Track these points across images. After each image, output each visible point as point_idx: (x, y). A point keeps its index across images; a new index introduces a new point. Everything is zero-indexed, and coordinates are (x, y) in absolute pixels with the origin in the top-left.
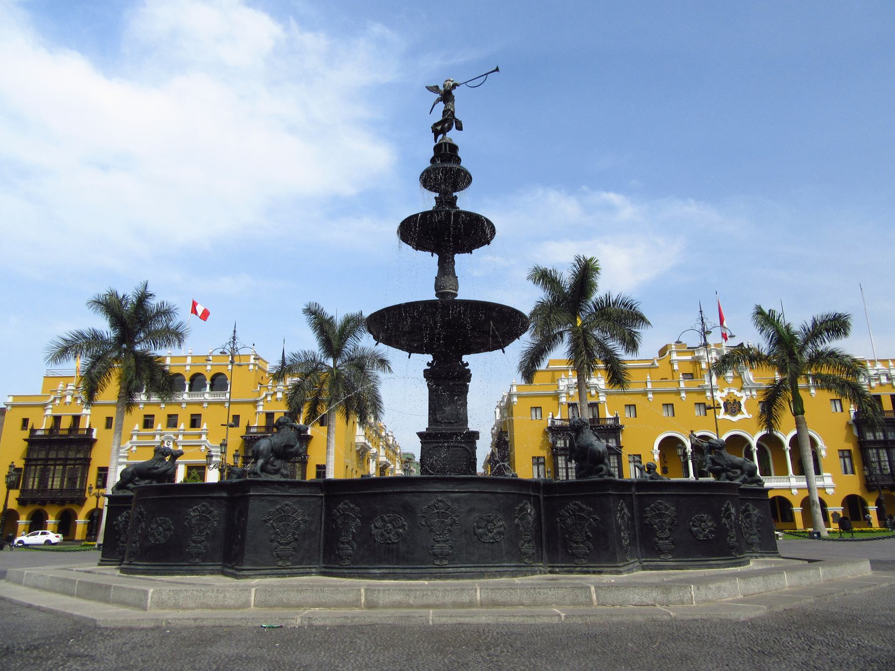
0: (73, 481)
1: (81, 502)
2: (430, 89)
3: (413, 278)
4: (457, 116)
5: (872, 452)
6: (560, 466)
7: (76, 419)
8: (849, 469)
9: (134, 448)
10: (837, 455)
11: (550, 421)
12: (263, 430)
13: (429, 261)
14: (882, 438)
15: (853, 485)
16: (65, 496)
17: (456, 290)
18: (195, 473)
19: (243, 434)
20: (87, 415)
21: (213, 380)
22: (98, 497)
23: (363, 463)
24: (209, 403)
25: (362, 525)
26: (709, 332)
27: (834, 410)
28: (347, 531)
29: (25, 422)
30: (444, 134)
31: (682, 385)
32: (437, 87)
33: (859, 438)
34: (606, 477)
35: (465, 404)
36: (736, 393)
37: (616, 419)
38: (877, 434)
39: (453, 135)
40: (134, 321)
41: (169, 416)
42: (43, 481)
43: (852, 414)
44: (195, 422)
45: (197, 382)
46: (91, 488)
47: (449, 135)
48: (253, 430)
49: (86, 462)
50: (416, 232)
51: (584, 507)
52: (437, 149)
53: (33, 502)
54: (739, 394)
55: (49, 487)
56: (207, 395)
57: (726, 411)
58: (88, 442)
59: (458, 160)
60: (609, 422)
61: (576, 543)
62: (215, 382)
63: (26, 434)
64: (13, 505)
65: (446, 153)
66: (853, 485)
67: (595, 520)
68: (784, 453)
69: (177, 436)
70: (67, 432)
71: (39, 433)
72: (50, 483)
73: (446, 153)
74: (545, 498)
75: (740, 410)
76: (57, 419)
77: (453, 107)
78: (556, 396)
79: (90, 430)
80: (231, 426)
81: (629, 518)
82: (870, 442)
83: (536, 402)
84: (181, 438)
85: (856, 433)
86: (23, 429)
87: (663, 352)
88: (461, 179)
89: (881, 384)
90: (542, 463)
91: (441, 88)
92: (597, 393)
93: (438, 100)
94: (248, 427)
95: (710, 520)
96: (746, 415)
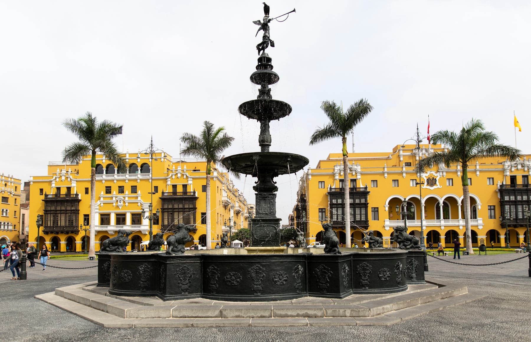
0: (71, 221)
1: (77, 232)
2: (255, 23)
3: (245, 137)
4: (271, 38)
5: (507, 207)
7: (69, 189)
9: (102, 204)
10: (487, 208)
11: (329, 189)
13: (255, 125)
14: (514, 199)
15: (493, 224)
16: (68, 229)
17: (270, 142)
18: (136, 220)
19: (160, 196)
21: (142, 167)
24: (141, 180)
25: (220, 278)
26: (421, 141)
28: (214, 279)
29: (41, 190)
30: (264, 51)
31: (404, 169)
32: (259, 21)
33: (501, 199)
34: (338, 254)
35: (273, 204)
37: (366, 188)
39: (269, 51)
40: (95, 135)
41: (119, 187)
42: (55, 222)
43: (499, 186)
44: (134, 189)
45: (133, 168)
46: (81, 226)
47: (266, 51)
48: (165, 194)
49: (77, 212)
50: (248, 109)
51: (322, 276)
52: (260, 60)
53: (52, 233)
54: (436, 175)
55: (59, 225)
56: (139, 175)
57: (428, 184)
59: (272, 67)
60: (362, 190)
61: (322, 283)
62: (143, 168)
63: (43, 197)
64: (41, 234)
65: (265, 62)
66: (493, 224)
67: (331, 273)
68: (458, 207)
69: (125, 198)
70: (64, 196)
71: (49, 197)
72: (59, 223)
73: (265, 62)
74: (308, 262)
75: (435, 184)
76: (59, 189)
77: (269, 34)
78: (333, 175)
79: (77, 195)
80: (154, 193)
81: (348, 271)
82: (507, 201)
84: (127, 199)
85: (499, 197)
86: (41, 194)
87: (395, 150)
88: (272, 78)
89: (517, 169)
91: (262, 22)
92: (356, 173)
93: (259, 30)
94: (163, 193)
95: (389, 271)
96: (439, 187)
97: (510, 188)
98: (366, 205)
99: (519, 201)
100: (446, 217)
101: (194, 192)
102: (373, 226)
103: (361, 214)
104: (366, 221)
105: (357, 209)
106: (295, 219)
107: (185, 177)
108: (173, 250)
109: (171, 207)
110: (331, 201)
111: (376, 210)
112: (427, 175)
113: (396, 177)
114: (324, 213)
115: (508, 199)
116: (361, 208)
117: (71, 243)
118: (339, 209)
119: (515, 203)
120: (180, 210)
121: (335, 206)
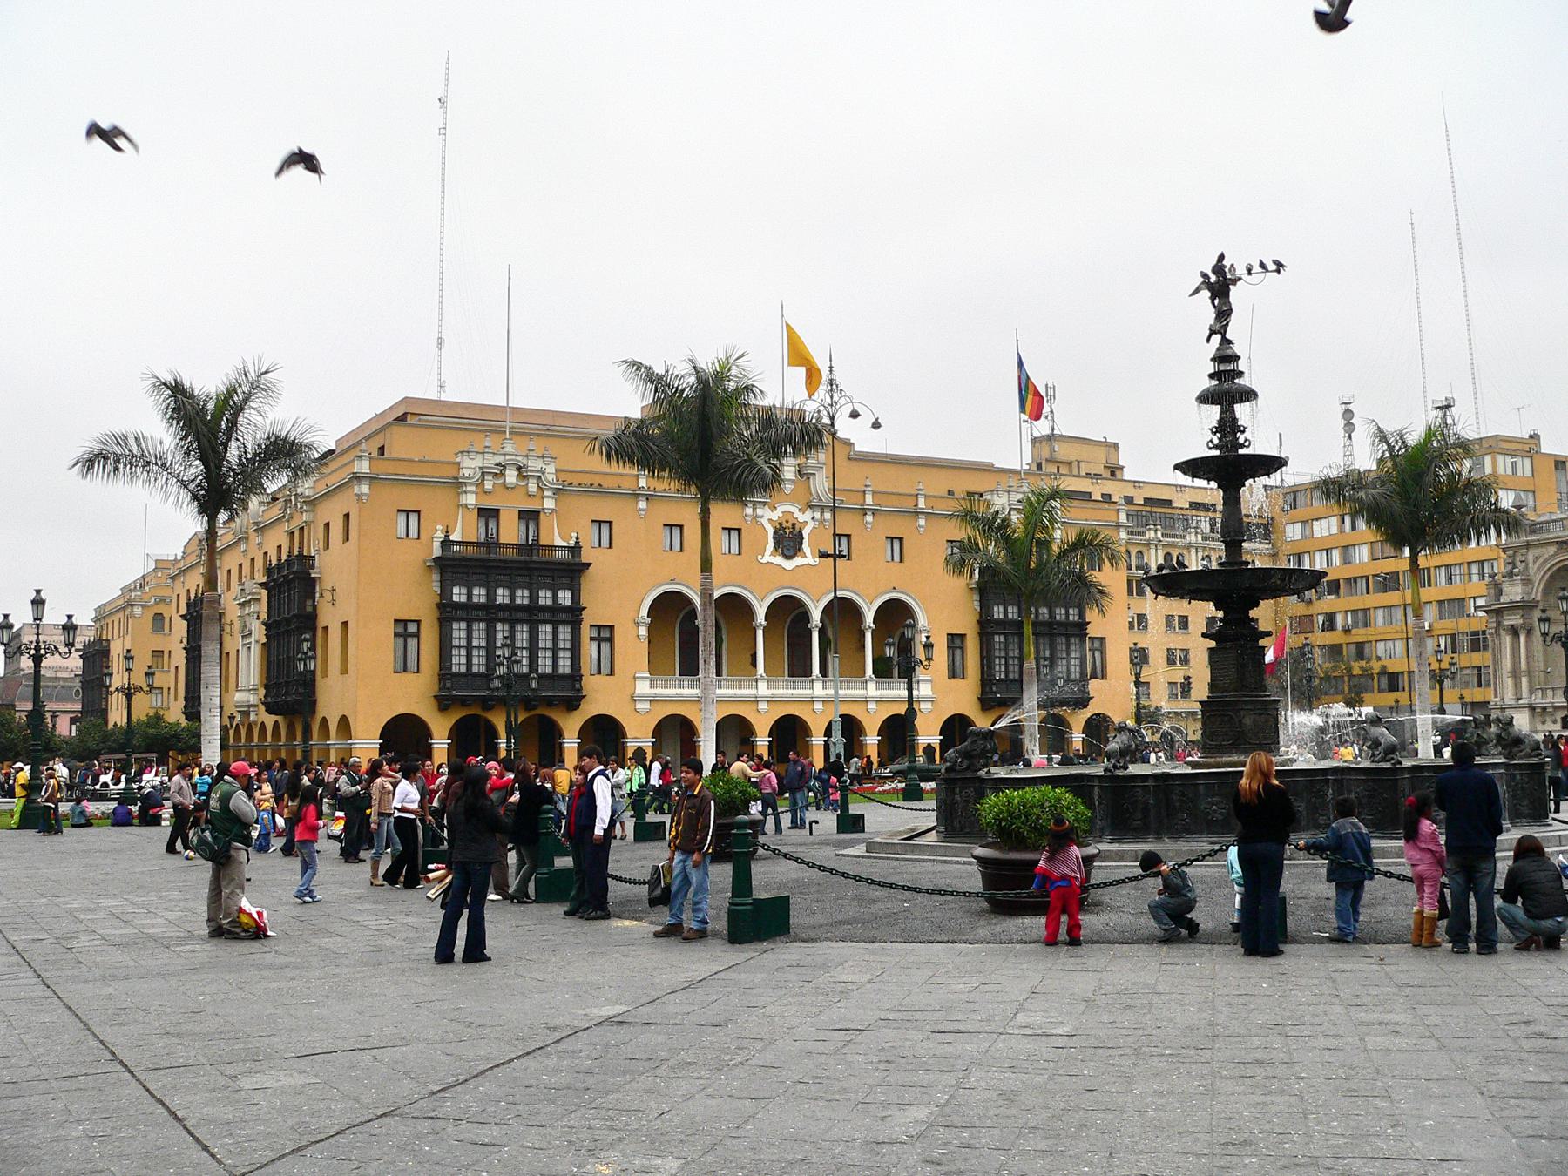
6: (456, 643)
8: (412, 664)
11: (437, 544)
14: (568, 602)
15: (413, 695)
22: (129, 696)
23: (162, 629)
27: (401, 531)
36: (797, 514)
37: (575, 550)
38: (561, 594)
53: (463, 702)
54: (801, 517)
60: (560, 555)
65: (1225, 356)
66: (413, 695)
82: (999, 622)
83: (410, 499)
88: (1249, 395)
90: (605, 640)
97: (516, 557)
98: (573, 615)
102: (601, 698)
103: (555, 650)
104: (575, 676)
108: (1115, 767)
110: (445, 592)
111: (605, 634)
112: (775, 515)
113: (897, 527)
114: (412, 643)
115: (464, 599)
116: (470, 622)
118: (475, 626)
119: (489, 613)
120: (562, 616)
121: (506, 615)
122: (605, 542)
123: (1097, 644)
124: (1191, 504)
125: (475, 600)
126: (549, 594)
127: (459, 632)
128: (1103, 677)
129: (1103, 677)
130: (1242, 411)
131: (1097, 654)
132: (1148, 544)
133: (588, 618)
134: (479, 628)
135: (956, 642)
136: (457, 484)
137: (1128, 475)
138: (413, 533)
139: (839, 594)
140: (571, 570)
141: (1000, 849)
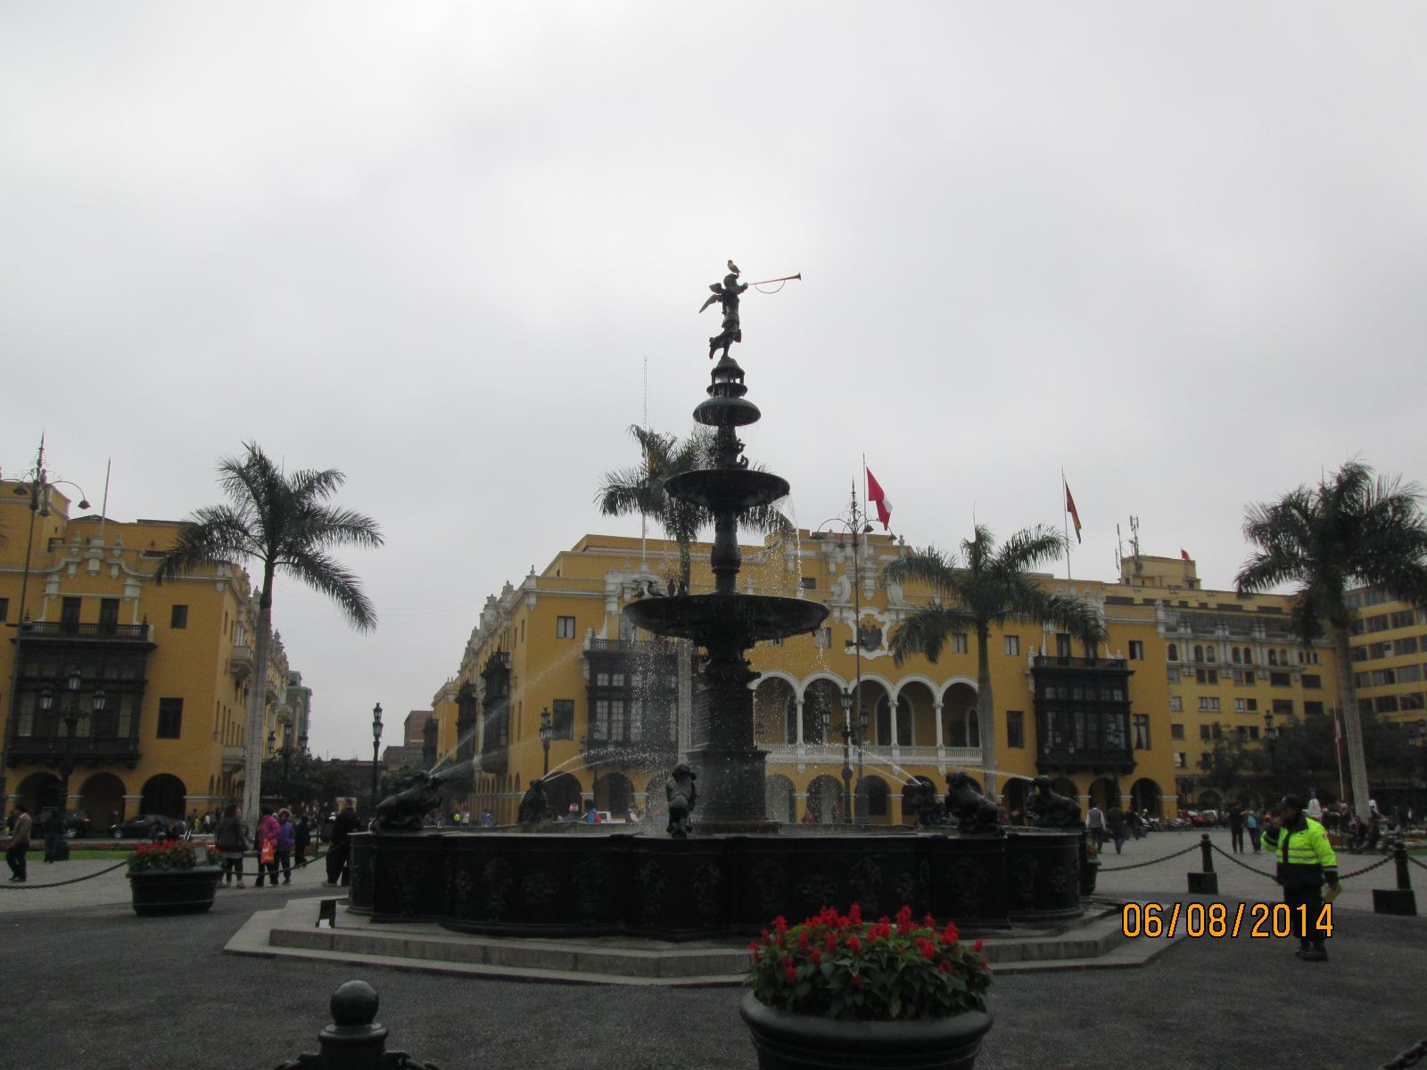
7: (110, 605)
12: (55, 629)
20: (133, 599)
39: (735, 351)
49: (138, 687)
54: (880, 618)
58: (140, 650)
59: (743, 389)
65: (728, 374)
68: (933, 711)
70: (94, 631)
73: (728, 374)
76: (71, 604)
85: (1032, 688)
88: (750, 415)
90: (1142, 724)
98: (1124, 707)
99: (603, 688)
100: (812, 735)
101: (144, 628)
105: (1076, 715)
106: (1229, 729)
107: (115, 572)
109: (606, 683)
117: (105, 792)
118: (615, 704)
122: (570, 634)
123: (1142, 720)
124: (1145, 600)
125: (615, 684)
126: (606, 677)
127: (602, 707)
128: (1148, 748)
129: (1148, 748)
130: (741, 432)
131: (1143, 729)
132: (1217, 641)
133: (1134, 709)
134: (618, 707)
135: (1014, 719)
136: (604, 598)
137: (1204, 586)
138: (570, 634)
139: (863, 678)
140: (1118, 675)
141: (205, 903)
